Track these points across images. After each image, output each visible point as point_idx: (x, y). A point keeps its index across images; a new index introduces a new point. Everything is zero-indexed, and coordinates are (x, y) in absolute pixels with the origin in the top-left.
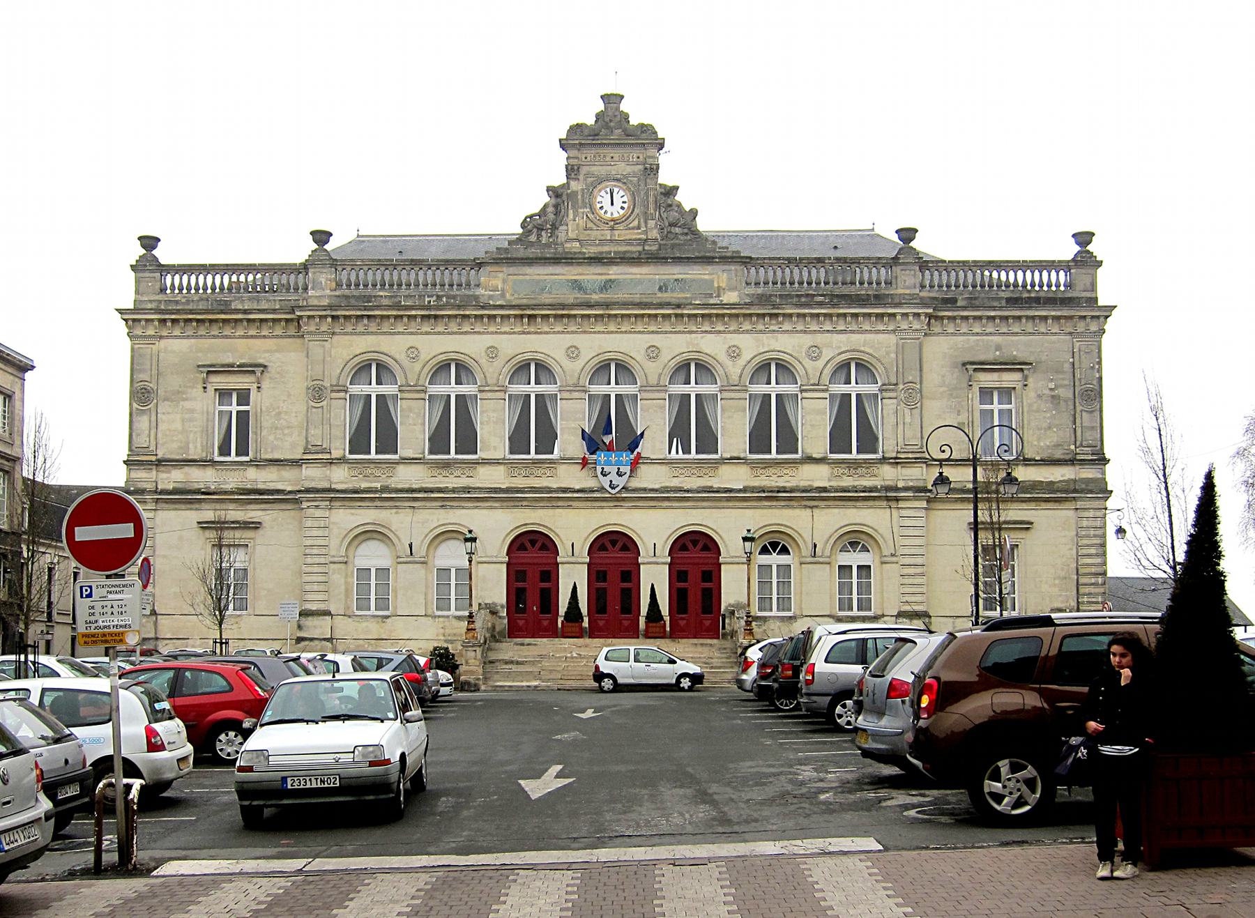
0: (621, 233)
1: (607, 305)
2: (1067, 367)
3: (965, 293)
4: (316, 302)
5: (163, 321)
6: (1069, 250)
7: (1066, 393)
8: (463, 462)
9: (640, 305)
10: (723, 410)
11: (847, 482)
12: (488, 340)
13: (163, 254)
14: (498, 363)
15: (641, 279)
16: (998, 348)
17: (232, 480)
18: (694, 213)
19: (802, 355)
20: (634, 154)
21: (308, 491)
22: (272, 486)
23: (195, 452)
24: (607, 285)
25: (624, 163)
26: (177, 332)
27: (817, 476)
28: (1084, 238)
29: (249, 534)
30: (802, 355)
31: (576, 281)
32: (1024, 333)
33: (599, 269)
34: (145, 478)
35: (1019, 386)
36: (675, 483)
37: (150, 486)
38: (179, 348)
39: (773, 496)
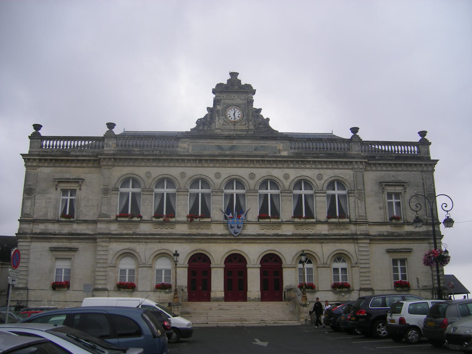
0: (238, 127)
1: (233, 156)
2: (421, 184)
6: (417, 138)
11: (336, 232)
12: (181, 170)
13: (43, 132)
14: (185, 180)
15: (246, 146)
16: (393, 176)
20: (243, 96)
22: (84, 232)
23: (50, 216)
24: (232, 148)
25: (238, 99)
27: (323, 229)
28: (423, 134)
31: (219, 146)
34: (28, 227)
35: (403, 192)
36: (262, 232)
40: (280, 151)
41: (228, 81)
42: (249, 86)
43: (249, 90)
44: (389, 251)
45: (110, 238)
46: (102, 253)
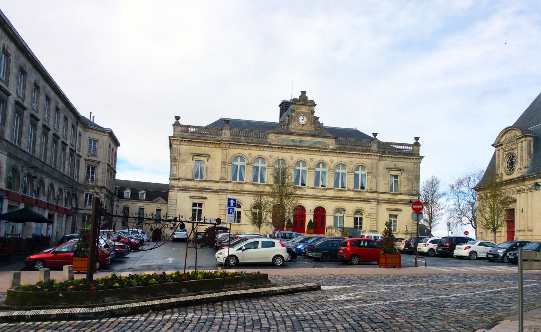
0: (305, 128)
1: (301, 147)
3: (387, 150)
4: (225, 139)
5: (182, 140)
6: (413, 141)
7: (411, 177)
8: (262, 185)
9: (309, 147)
10: (329, 176)
11: (358, 196)
12: (270, 153)
13: (181, 122)
14: (272, 159)
15: (310, 140)
17: (199, 185)
18: (323, 124)
19: (348, 163)
20: (309, 108)
21: (221, 190)
22: (210, 188)
23: (189, 177)
24: (301, 141)
25: (305, 109)
26: (185, 144)
27: (351, 194)
28: (417, 139)
29: (203, 200)
30: (348, 163)
32: (402, 162)
33: (299, 137)
34: (175, 183)
35: (400, 175)
36: (316, 194)
37: (176, 186)
38: (185, 148)
39: (340, 199)
40: (329, 145)
41: (300, 97)
42: (312, 102)
43: (312, 104)
44: (388, 210)
45: (227, 193)
46: (222, 201)
